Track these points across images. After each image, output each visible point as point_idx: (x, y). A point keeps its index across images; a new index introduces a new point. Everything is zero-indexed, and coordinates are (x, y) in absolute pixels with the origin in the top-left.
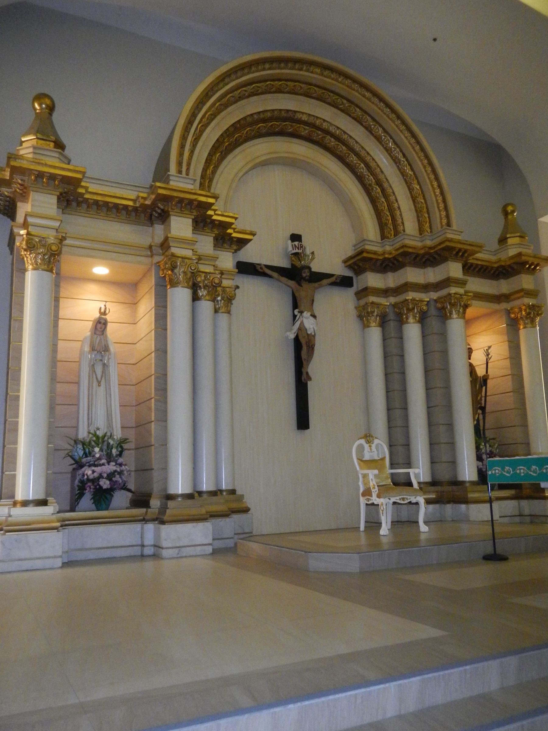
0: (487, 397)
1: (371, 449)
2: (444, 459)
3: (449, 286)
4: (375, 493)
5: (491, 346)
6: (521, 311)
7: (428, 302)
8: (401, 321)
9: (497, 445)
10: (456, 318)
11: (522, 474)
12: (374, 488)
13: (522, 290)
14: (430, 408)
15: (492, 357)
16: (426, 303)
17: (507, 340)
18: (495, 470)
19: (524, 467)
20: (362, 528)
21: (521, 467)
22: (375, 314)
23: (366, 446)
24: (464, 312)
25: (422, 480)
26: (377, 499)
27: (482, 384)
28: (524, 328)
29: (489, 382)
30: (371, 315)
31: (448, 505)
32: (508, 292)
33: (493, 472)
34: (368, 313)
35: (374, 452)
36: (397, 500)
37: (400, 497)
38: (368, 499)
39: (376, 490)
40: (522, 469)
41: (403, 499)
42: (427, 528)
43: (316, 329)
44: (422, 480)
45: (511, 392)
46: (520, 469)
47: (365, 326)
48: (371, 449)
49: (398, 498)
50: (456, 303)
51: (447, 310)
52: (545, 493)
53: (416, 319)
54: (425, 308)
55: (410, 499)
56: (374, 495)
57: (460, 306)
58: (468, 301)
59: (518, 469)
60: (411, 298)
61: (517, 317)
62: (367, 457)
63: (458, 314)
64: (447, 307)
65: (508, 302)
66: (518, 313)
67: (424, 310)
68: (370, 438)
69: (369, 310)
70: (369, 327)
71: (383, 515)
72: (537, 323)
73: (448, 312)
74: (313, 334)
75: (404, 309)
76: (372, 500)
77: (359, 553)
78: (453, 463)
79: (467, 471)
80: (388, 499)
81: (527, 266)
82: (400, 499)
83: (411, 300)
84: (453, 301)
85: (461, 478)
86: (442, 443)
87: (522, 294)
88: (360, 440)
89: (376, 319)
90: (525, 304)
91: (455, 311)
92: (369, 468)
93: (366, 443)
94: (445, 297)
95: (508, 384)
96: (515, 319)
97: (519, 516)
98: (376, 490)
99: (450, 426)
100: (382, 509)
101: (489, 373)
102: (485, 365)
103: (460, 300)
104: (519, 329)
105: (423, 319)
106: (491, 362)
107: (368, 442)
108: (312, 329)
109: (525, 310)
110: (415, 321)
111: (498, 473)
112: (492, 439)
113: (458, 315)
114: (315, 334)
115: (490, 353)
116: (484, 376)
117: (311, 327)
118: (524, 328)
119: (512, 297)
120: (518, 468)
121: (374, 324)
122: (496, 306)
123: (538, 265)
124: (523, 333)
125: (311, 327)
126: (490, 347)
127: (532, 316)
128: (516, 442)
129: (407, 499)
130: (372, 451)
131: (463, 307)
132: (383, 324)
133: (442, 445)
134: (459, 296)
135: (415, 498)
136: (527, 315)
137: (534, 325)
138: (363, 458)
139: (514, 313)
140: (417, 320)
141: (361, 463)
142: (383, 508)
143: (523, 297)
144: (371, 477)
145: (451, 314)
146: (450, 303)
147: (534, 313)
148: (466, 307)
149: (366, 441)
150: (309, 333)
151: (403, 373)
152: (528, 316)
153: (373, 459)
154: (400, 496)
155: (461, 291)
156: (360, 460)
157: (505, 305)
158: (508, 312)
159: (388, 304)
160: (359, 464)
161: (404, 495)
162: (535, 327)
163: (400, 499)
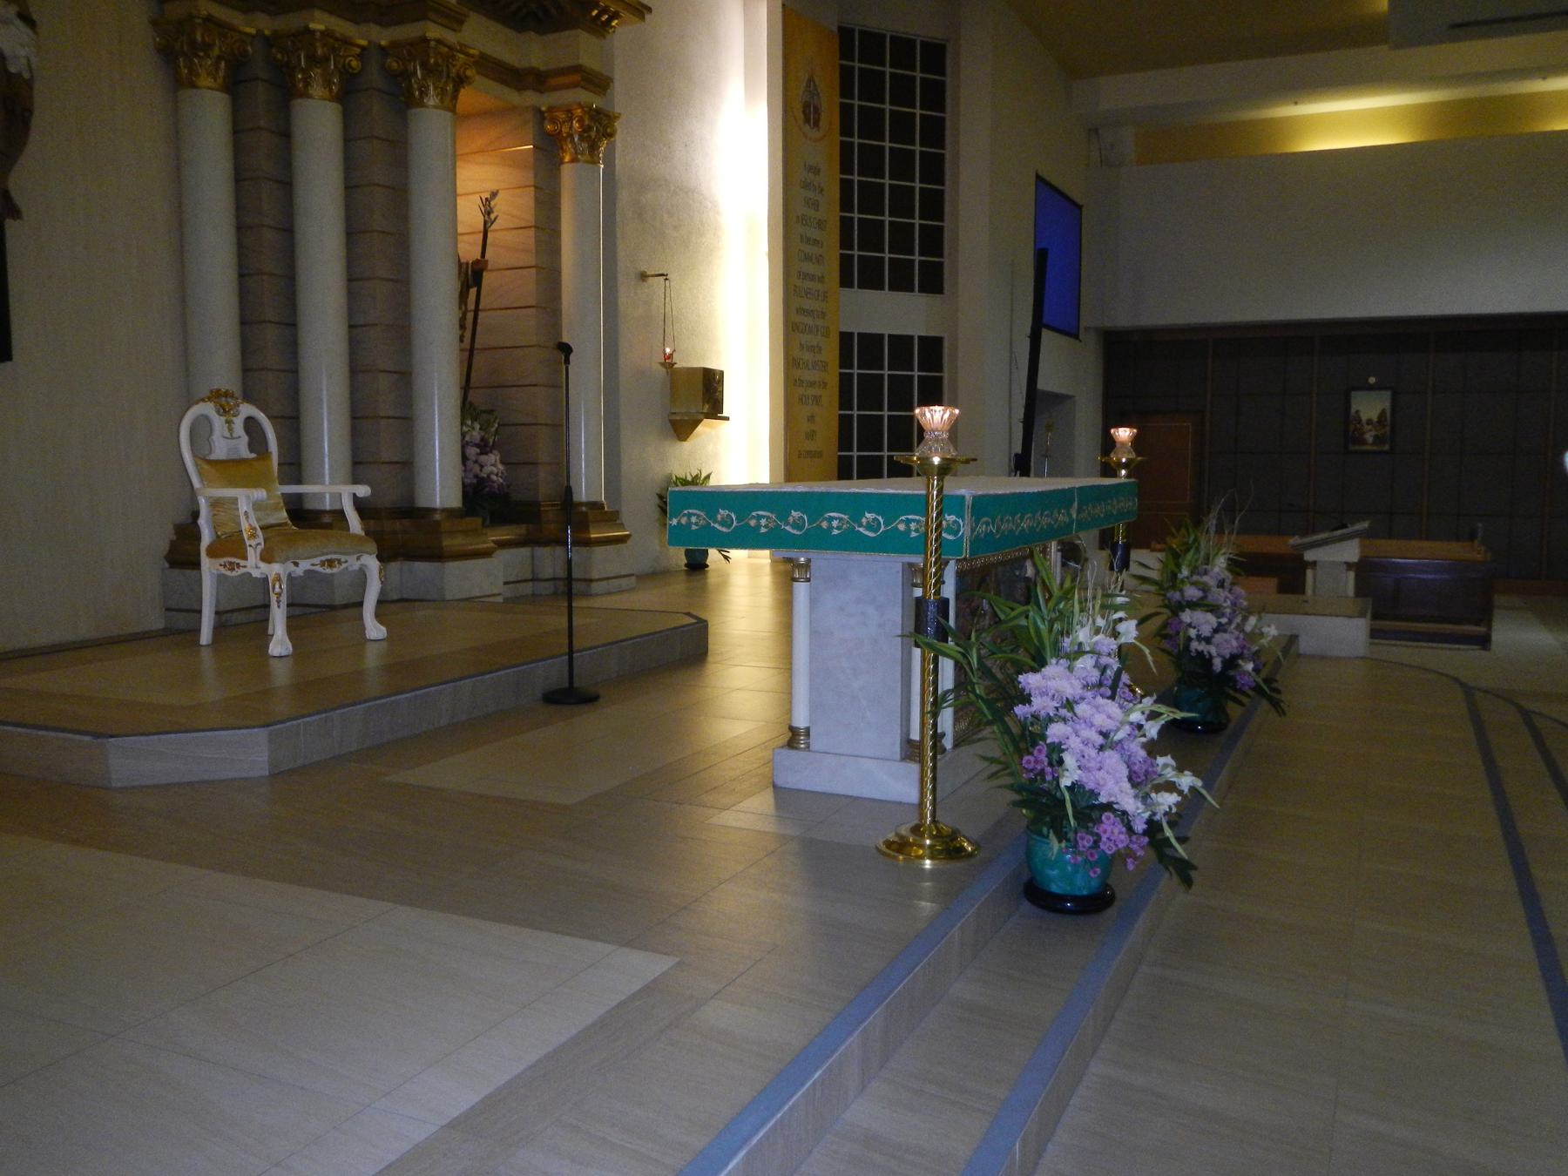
0: (480, 313)
1: (231, 430)
2: (386, 455)
3: (424, 18)
4: (255, 549)
5: (498, 191)
6: (571, 120)
7: (363, 48)
8: (287, 91)
9: (496, 425)
10: (435, 107)
11: (763, 530)
12: (253, 536)
13: (577, 69)
14: (355, 329)
15: (497, 221)
16: (358, 51)
17: (532, 183)
18: (689, 515)
19: (772, 512)
20: (206, 636)
21: (760, 513)
22: (216, 52)
23: (218, 422)
24: (455, 97)
25: (328, 504)
26: (262, 565)
27: (470, 282)
28: (574, 160)
29: (487, 278)
30: (201, 54)
31: (393, 564)
32: (542, 67)
33: (684, 521)
34: (193, 44)
35: (240, 437)
36: (313, 565)
37: (324, 558)
38: (231, 563)
39: (258, 541)
40: (763, 517)
41: (331, 563)
42: (384, 629)
43: (34, 60)
44: (328, 504)
45: (533, 307)
46: (759, 517)
47: (180, 83)
48: (231, 430)
49: (317, 561)
50: (440, 69)
51: (413, 81)
52: (589, 532)
53: (331, 89)
54: (354, 63)
55: (346, 562)
56: (253, 556)
57: (448, 77)
58: (466, 69)
59: (753, 517)
60: (322, 27)
61: (561, 131)
62: (220, 450)
63: (442, 98)
64: (415, 73)
65: (542, 92)
66: (564, 122)
67: (353, 69)
68: (229, 400)
69: (199, 38)
70: (193, 86)
71: (279, 607)
72: (601, 155)
73: (415, 86)
74: (26, 75)
75: (299, 56)
76: (245, 567)
77: (268, 726)
78: (407, 466)
79: (327, 466)
80: (292, 565)
81: (595, 13)
82: (322, 564)
83: (322, 33)
84: (432, 61)
85: (422, 502)
86: (383, 417)
87: (577, 78)
88: (202, 405)
89: (217, 69)
90: (582, 103)
91: (435, 88)
92: (232, 483)
93: (218, 412)
94: (411, 45)
95: (526, 287)
96: (552, 135)
97: (531, 580)
98: (258, 541)
99: (404, 377)
100: (277, 590)
101: (487, 256)
102: (481, 235)
103: (448, 61)
104: (562, 162)
105: (347, 93)
106: (493, 231)
107: (224, 411)
108: (24, 61)
109: (581, 121)
110: (328, 93)
111: (696, 524)
112: (484, 412)
113: (442, 101)
114: (32, 77)
115: (494, 210)
116: (477, 262)
117: (22, 52)
118: (574, 160)
119: (553, 82)
120: (754, 514)
121: (209, 82)
122: (513, 97)
123: (615, 16)
124: (568, 172)
125: (22, 52)
126: (494, 194)
127: (593, 134)
128: (534, 421)
129: (339, 562)
130: (234, 436)
131: (454, 80)
132: (234, 86)
133: (383, 422)
134: (446, 49)
135: (358, 559)
136: (584, 131)
137: (596, 158)
138: (210, 453)
139: (553, 121)
140: (333, 94)
141: (206, 467)
142: (280, 587)
143: (575, 85)
144: (243, 506)
145: (423, 93)
146: (424, 65)
147: (598, 130)
148: (461, 81)
149: (218, 407)
150: (13, 69)
151: (288, 230)
152: (586, 135)
153: (235, 457)
154: (323, 554)
155: (451, 37)
156: (202, 458)
157: (530, 98)
158: (540, 116)
159: (253, 31)
160: (200, 473)
161: (331, 553)
162: (596, 163)
163: (322, 564)
